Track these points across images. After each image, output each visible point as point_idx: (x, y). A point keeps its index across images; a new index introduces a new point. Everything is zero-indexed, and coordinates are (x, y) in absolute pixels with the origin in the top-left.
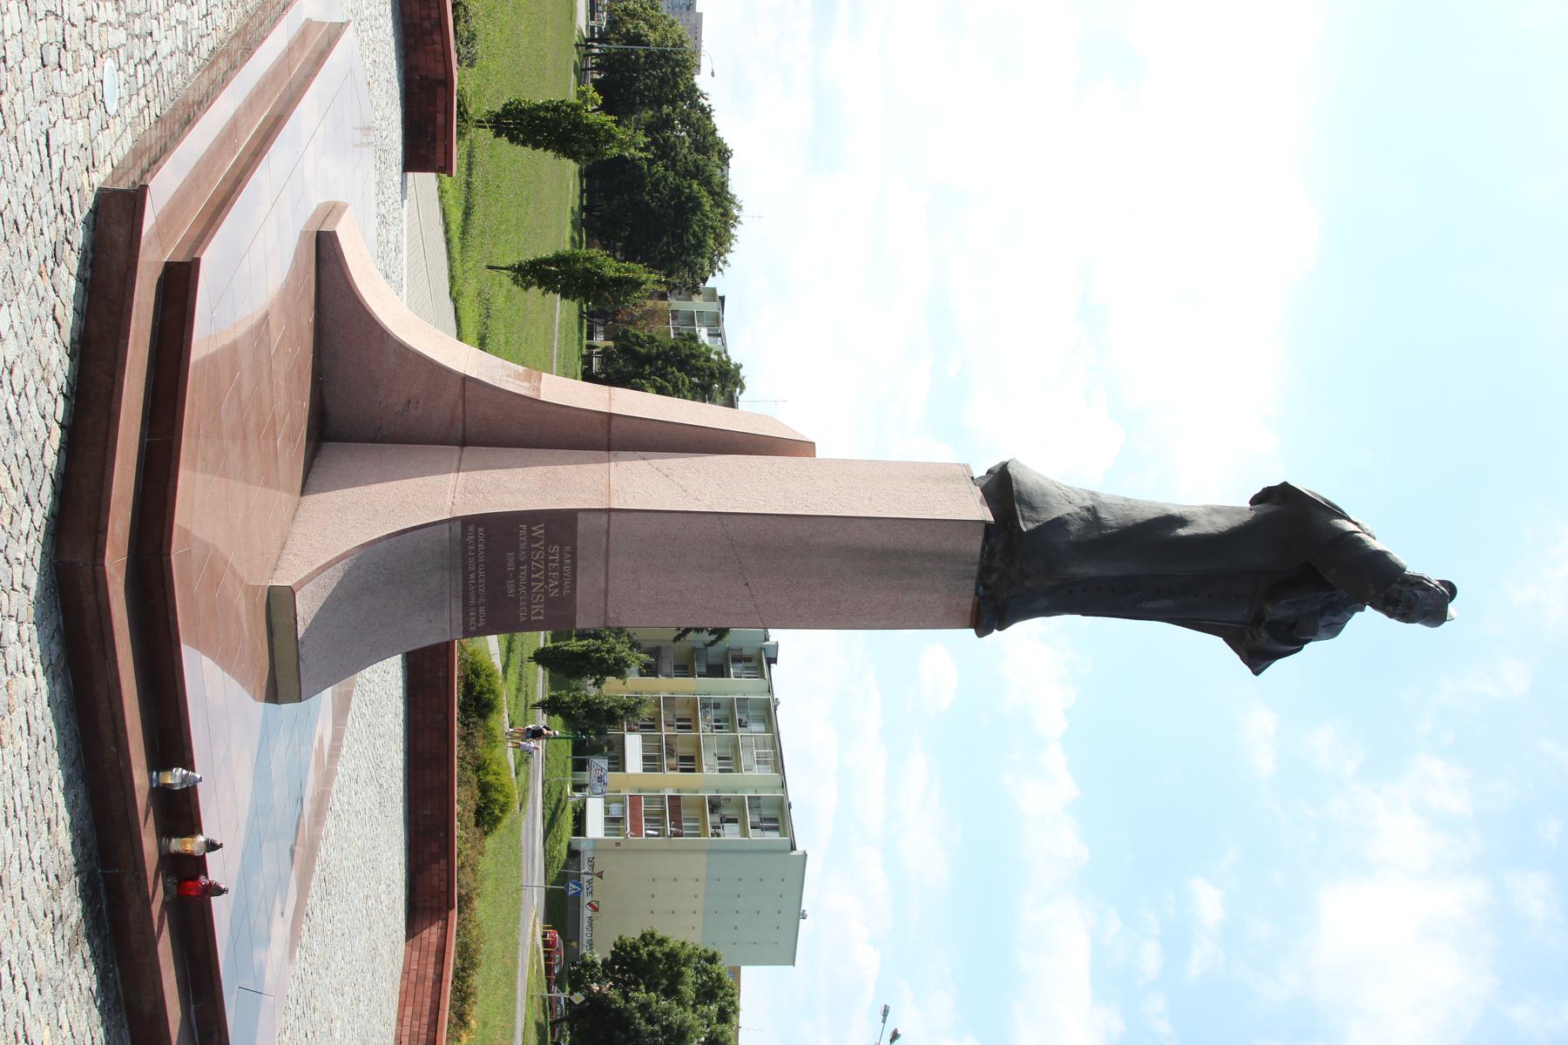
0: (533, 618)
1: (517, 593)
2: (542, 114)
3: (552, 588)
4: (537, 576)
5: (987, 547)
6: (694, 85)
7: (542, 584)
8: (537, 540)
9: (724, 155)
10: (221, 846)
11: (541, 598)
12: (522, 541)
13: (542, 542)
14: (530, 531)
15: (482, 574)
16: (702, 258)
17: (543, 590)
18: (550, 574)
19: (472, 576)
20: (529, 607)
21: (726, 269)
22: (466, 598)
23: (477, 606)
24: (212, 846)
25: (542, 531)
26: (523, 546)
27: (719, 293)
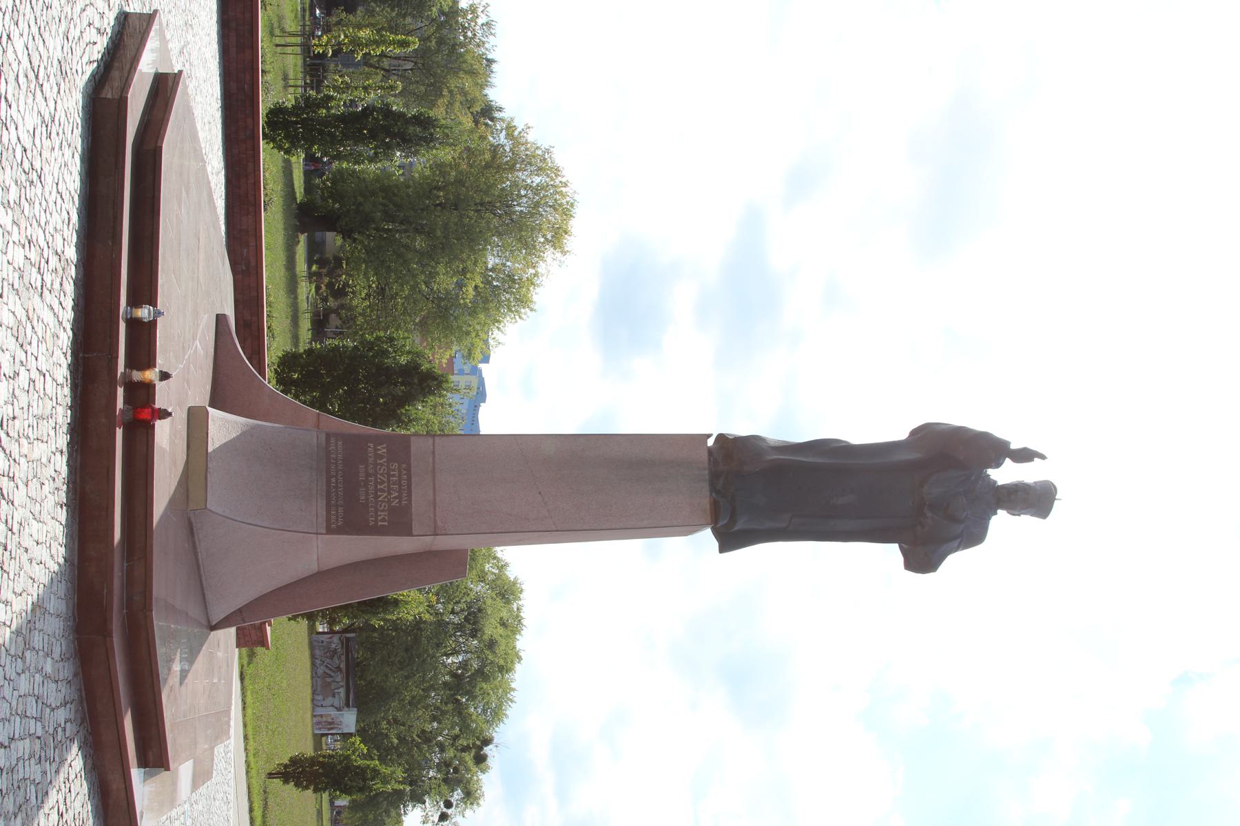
0: (380, 523)
1: (367, 499)
2: (321, 759)
3: (393, 498)
4: (382, 487)
5: (712, 459)
7: (385, 494)
8: (381, 457)
10: (170, 414)
11: (385, 506)
12: (370, 457)
13: (385, 460)
14: (376, 450)
15: (341, 479)
17: (386, 500)
18: (392, 486)
19: (333, 480)
20: (376, 513)
23: (337, 506)
24: (165, 376)
25: (385, 450)
26: (371, 460)
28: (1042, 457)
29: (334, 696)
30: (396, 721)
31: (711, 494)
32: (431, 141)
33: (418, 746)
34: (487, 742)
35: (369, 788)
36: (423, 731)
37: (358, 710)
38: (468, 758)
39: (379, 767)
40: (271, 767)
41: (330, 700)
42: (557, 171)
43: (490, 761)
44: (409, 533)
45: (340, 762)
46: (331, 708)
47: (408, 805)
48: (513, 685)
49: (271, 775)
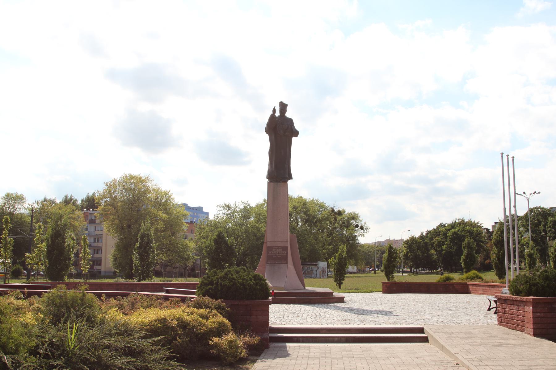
2: (335, 272)
6: (419, 237)
8: (271, 253)
9: (441, 225)
16: (474, 231)
21: (481, 222)
22: (280, 264)
26: (272, 255)
27: (494, 224)
28: (275, 107)
29: (313, 270)
30: (323, 246)
31: (280, 182)
32: (148, 234)
33: (333, 238)
34: (333, 210)
35: (345, 257)
36: (328, 235)
37: (319, 261)
38: (339, 218)
39: (339, 254)
40: (337, 287)
41: (314, 272)
42: (114, 181)
43: (341, 209)
44: (287, 247)
45: (337, 266)
46: (317, 271)
47: (357, 242)
48: (311, 199)
49: (340, 288)
